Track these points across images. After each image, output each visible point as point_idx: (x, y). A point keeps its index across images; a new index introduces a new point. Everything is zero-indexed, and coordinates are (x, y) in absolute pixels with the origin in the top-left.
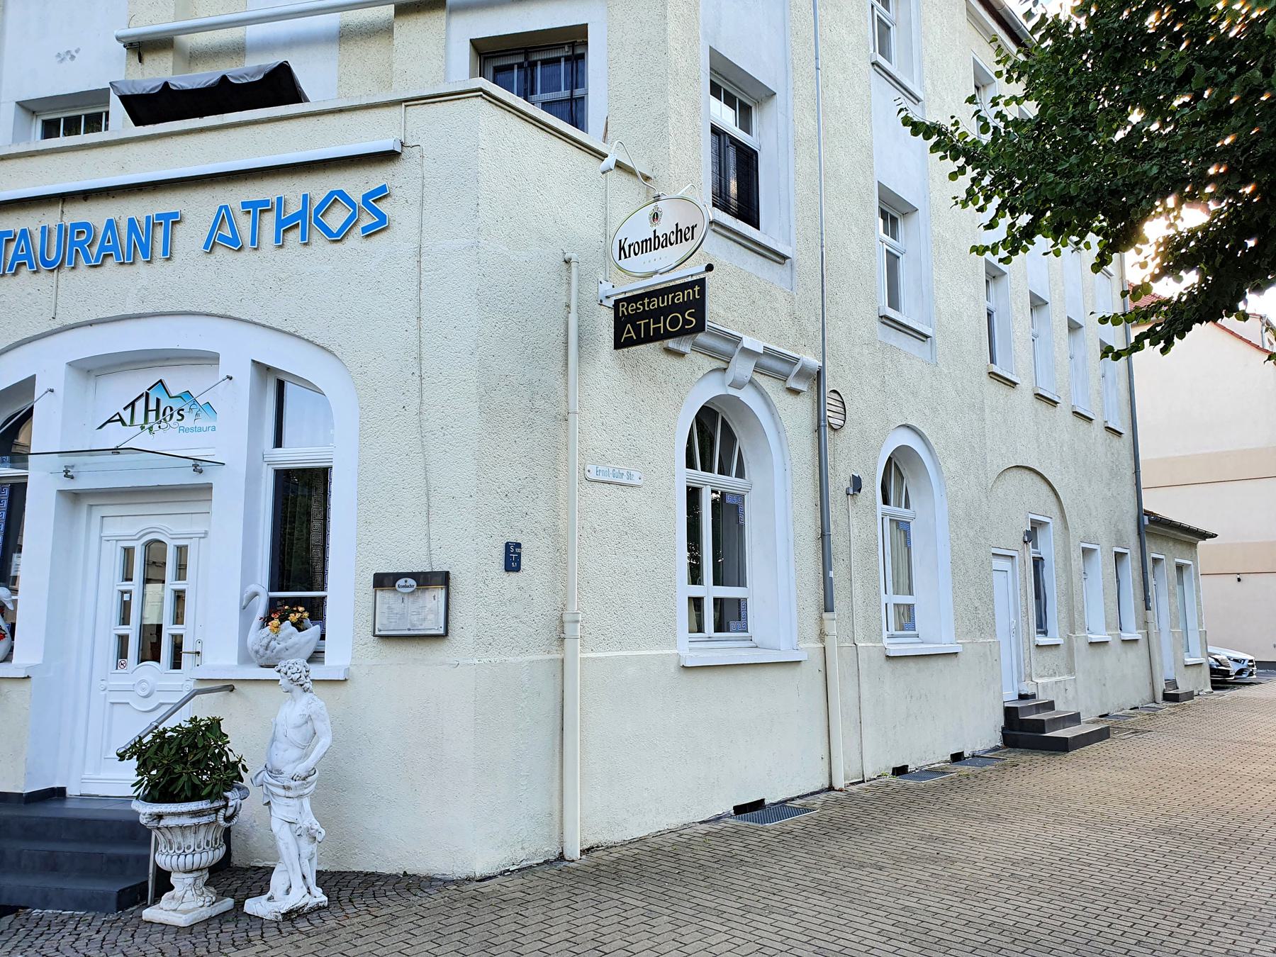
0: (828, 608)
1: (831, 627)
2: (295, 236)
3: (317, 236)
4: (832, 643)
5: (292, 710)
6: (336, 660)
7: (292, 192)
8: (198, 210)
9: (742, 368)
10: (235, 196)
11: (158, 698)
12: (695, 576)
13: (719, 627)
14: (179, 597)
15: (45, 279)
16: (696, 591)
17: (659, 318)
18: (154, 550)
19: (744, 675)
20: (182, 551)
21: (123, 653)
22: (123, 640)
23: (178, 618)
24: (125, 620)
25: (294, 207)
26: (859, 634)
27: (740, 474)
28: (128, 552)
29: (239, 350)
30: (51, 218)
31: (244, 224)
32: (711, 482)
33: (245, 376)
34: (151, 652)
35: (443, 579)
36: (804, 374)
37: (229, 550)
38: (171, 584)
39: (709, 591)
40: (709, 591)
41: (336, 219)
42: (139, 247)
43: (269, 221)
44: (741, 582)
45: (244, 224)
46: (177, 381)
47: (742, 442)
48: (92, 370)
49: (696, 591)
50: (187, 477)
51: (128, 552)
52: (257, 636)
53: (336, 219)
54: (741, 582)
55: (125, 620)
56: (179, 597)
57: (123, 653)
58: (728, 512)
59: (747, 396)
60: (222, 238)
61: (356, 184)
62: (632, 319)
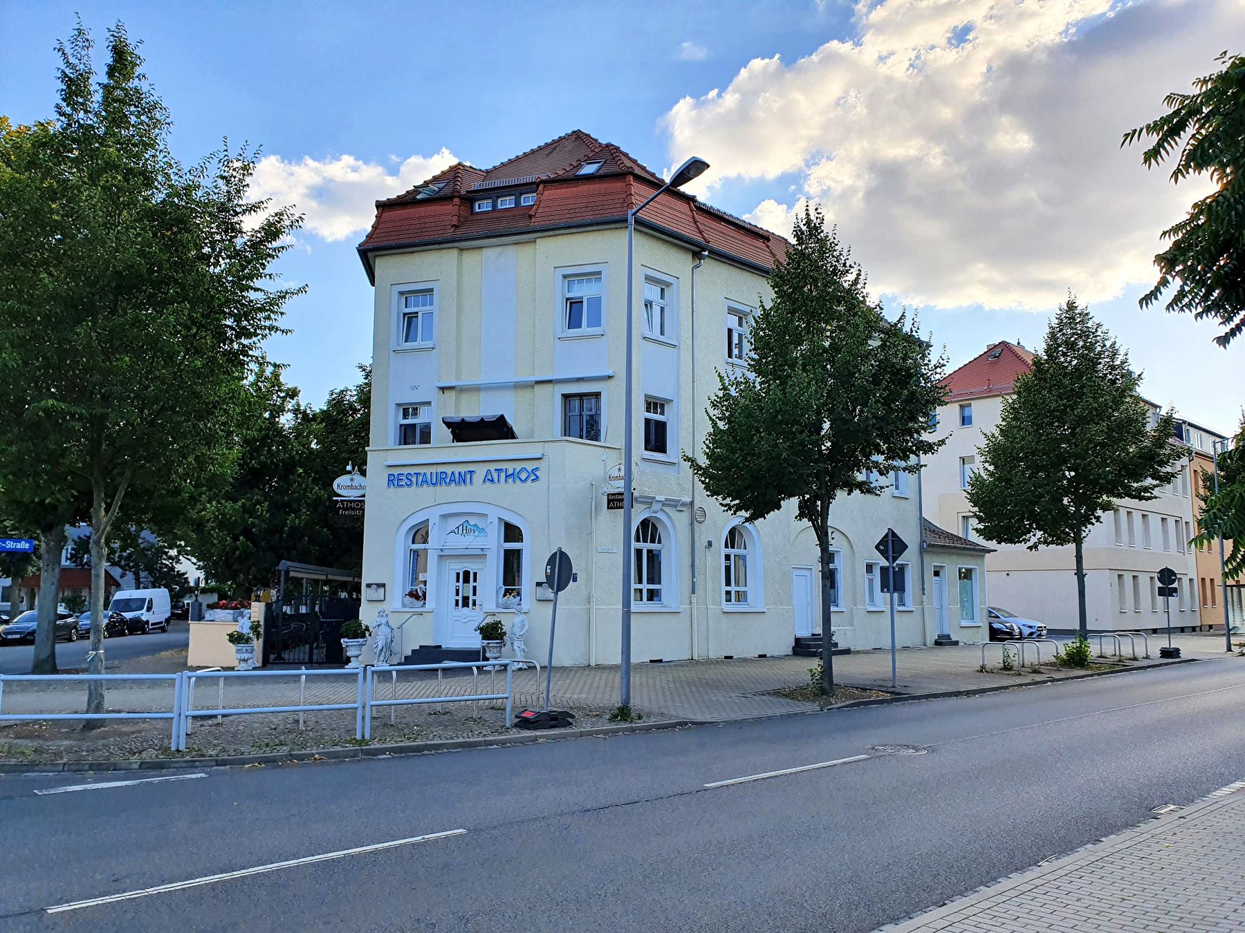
0: (693, 592)
1: (694, 600)
2: (510, 480)
3: (518, 481)
4: (695, 606)
5: (518, 619)
6: (525, 606)
7: (510, 467)
8: (481, 471)
9: (656, 507)
10: (492, 467)
11: (476, 617)
12: (728, 583)
13: (649, 600)
14: (475, 588)
15: (431, 488)
16: (728, 588)
17: (615, 502)
18: (467, 574)
19: (655, 616)
20: (475, 574)
21: (457, 604)
22: (457, 601)
23: (474, 594)
24: (457, 594)
25: (510, 472)
26: (709, 602)
27: (659, 542)
28: (458, 574)
29: (494, 515)
30: (433, 469)
31: (495, 475)
32: (646, 546)
33: (496, 522)
34: (465, 604)
35: (384, 585)
36: (684, 504)
37: (490, 575)
38: (472, 583)
39: (645, 586)
40: (645, 586)
41: (523, 476)
42: (462, 479)
43: (503, 475)
44: (659, 583)
45: (495, 475)
46: (472, 521)
47: (660, 530)
48: (445, 517)
49: (728, 588)
50: (479, 552)
51: (458, 574)
52: (502, 600)
53: (523, 476)
54: (659, 583)
55: (457, 594)
56: (475, 588)
57: (457, 604)
58: (654, 557)
59: (660, 515)
60: (489, 479)
61: (530, 466)
62: (613, 500)
